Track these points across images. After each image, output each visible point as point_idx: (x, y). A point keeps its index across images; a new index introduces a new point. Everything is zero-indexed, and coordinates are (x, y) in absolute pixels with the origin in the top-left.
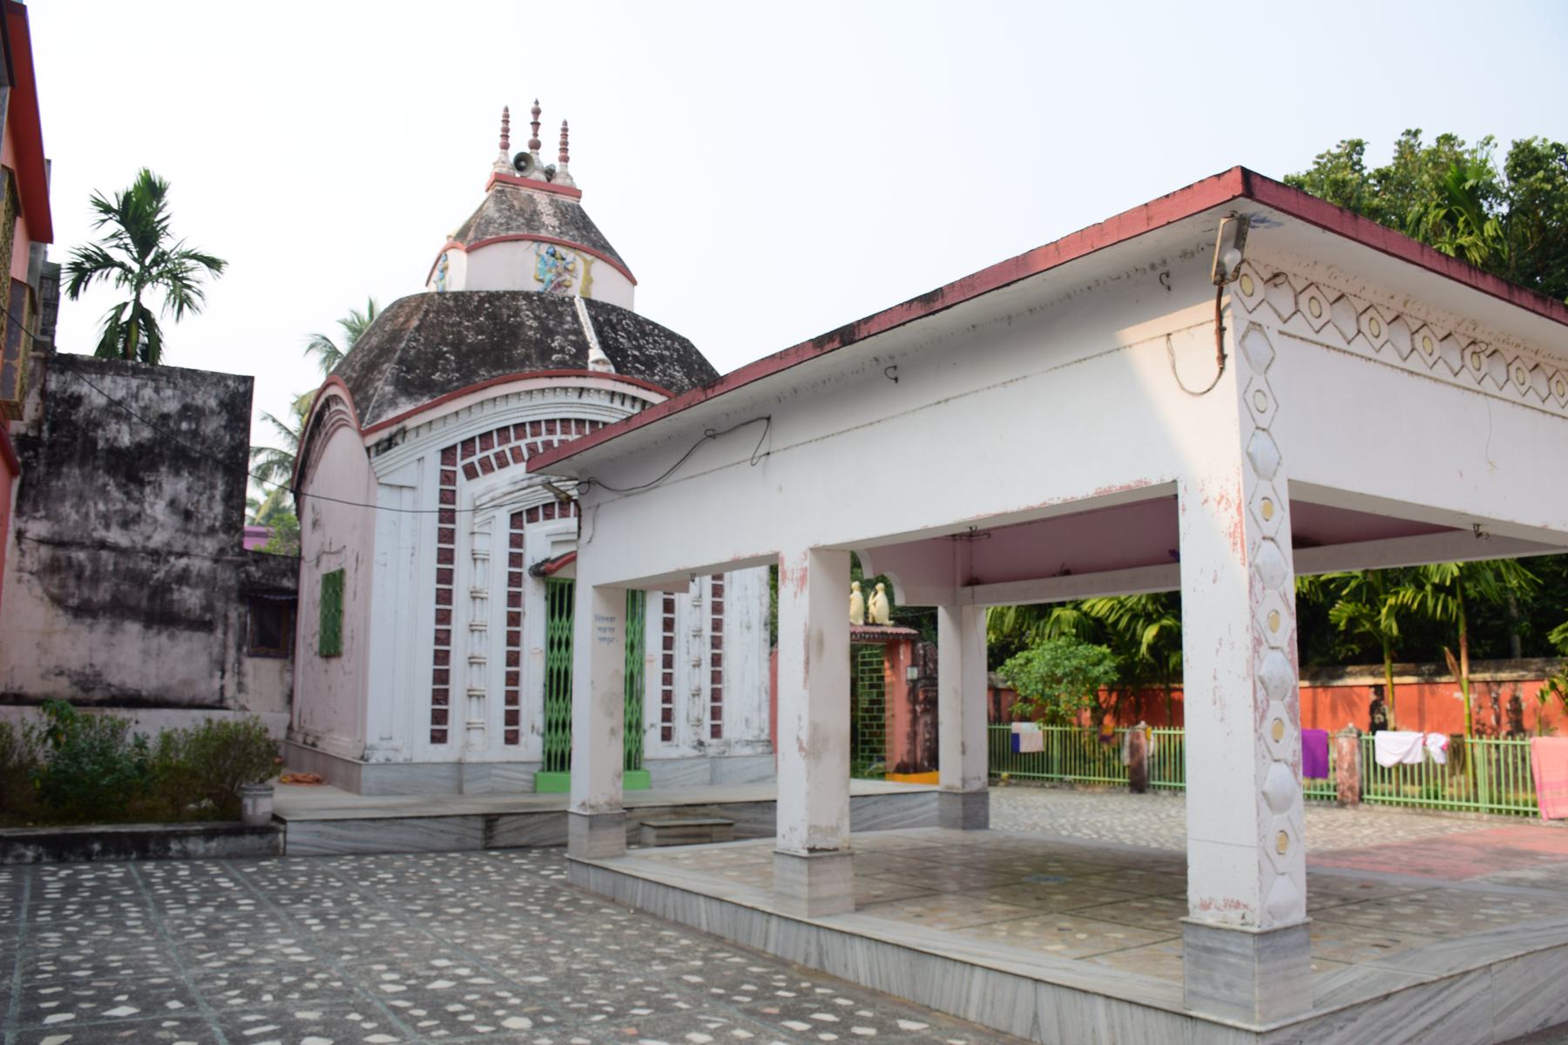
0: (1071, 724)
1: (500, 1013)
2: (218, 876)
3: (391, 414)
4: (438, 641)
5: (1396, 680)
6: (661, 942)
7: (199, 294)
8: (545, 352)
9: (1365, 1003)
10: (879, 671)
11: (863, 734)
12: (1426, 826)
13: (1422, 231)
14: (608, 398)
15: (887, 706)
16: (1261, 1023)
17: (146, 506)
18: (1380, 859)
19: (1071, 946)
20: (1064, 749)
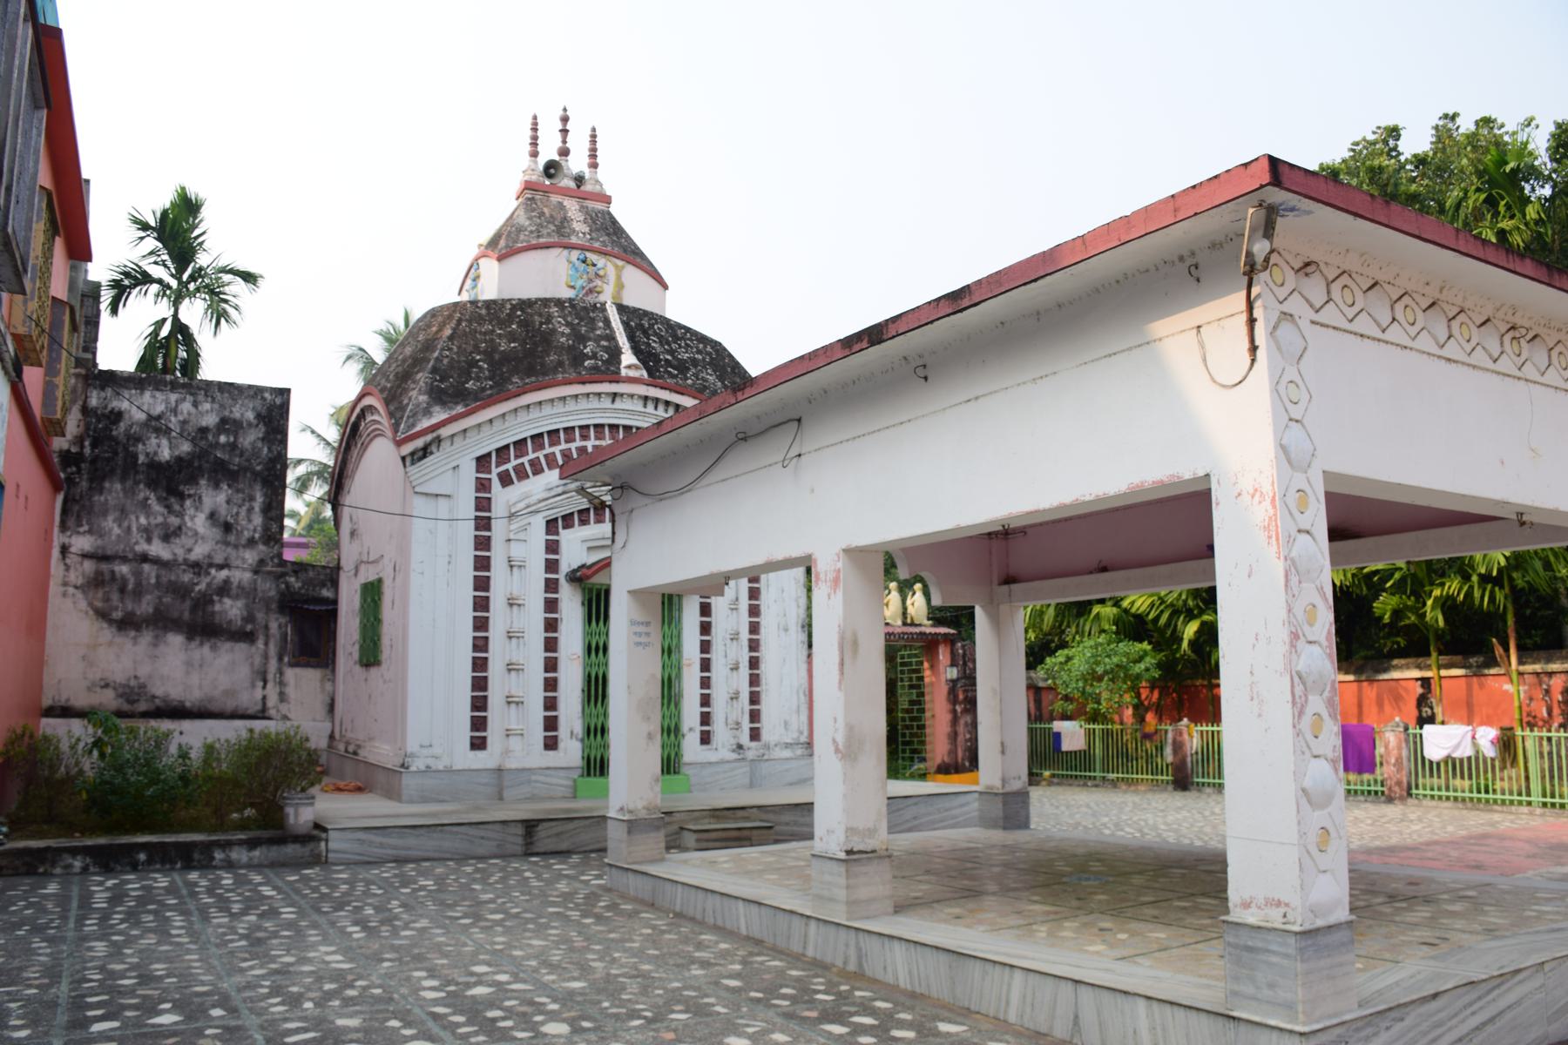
0: (1113, 723)
1: (539, 1018)
2: (261, 884)
3: (425, 423)
4: (476, 648)
5: (1443, 673)
6: (700, 946)
7: (236, 308)
8: (578, 359)
9: (1413, 1002)
10: (918, 671)
11: (904, 735)
12: (1476, 821)
13: (1462, 216)
14: (641, 403)
15: (927, 706)
16: (1304, 1024)
17: (187, 518)
18: (1430, 855)
19: (1111, 946)
20: (1106, 747)
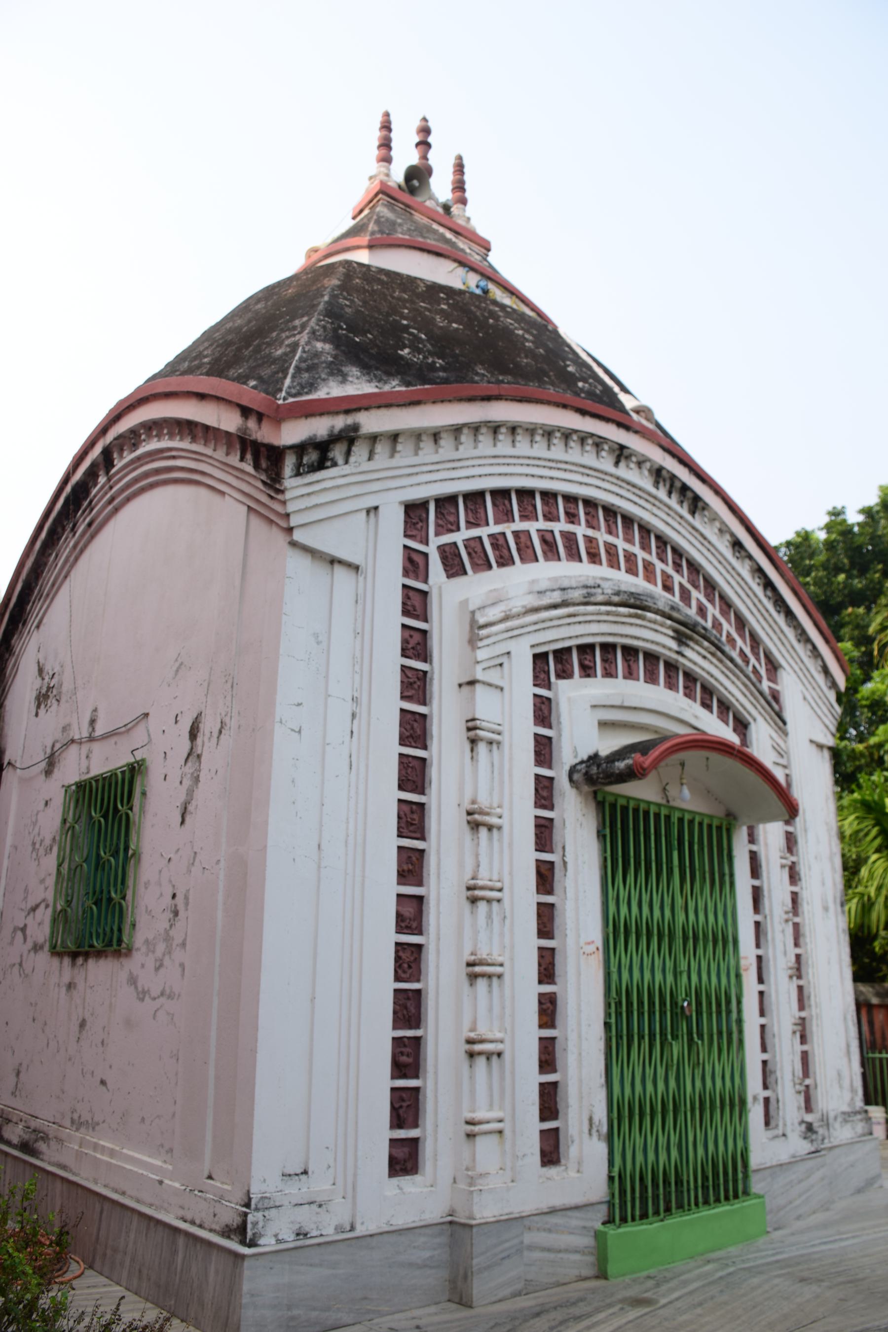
3: (332, 390)
